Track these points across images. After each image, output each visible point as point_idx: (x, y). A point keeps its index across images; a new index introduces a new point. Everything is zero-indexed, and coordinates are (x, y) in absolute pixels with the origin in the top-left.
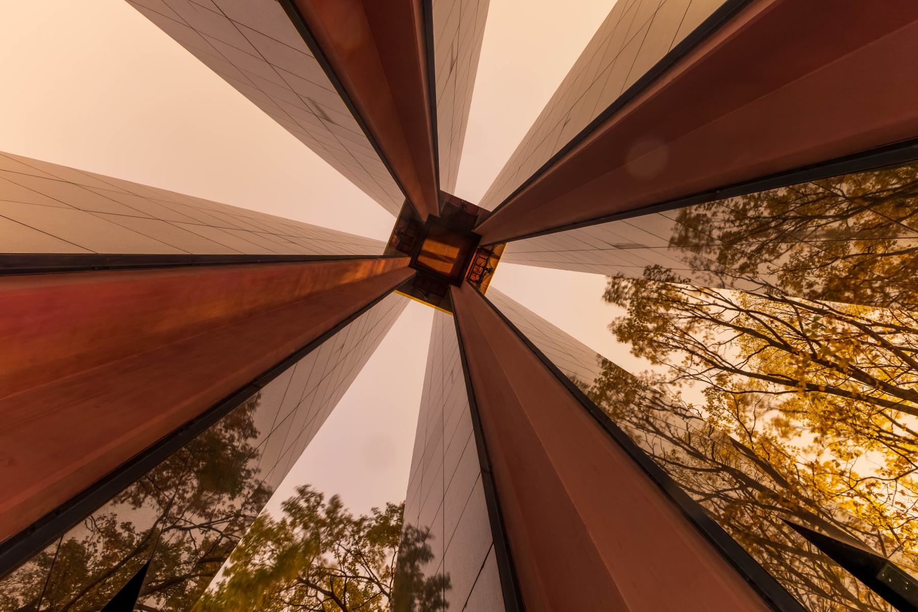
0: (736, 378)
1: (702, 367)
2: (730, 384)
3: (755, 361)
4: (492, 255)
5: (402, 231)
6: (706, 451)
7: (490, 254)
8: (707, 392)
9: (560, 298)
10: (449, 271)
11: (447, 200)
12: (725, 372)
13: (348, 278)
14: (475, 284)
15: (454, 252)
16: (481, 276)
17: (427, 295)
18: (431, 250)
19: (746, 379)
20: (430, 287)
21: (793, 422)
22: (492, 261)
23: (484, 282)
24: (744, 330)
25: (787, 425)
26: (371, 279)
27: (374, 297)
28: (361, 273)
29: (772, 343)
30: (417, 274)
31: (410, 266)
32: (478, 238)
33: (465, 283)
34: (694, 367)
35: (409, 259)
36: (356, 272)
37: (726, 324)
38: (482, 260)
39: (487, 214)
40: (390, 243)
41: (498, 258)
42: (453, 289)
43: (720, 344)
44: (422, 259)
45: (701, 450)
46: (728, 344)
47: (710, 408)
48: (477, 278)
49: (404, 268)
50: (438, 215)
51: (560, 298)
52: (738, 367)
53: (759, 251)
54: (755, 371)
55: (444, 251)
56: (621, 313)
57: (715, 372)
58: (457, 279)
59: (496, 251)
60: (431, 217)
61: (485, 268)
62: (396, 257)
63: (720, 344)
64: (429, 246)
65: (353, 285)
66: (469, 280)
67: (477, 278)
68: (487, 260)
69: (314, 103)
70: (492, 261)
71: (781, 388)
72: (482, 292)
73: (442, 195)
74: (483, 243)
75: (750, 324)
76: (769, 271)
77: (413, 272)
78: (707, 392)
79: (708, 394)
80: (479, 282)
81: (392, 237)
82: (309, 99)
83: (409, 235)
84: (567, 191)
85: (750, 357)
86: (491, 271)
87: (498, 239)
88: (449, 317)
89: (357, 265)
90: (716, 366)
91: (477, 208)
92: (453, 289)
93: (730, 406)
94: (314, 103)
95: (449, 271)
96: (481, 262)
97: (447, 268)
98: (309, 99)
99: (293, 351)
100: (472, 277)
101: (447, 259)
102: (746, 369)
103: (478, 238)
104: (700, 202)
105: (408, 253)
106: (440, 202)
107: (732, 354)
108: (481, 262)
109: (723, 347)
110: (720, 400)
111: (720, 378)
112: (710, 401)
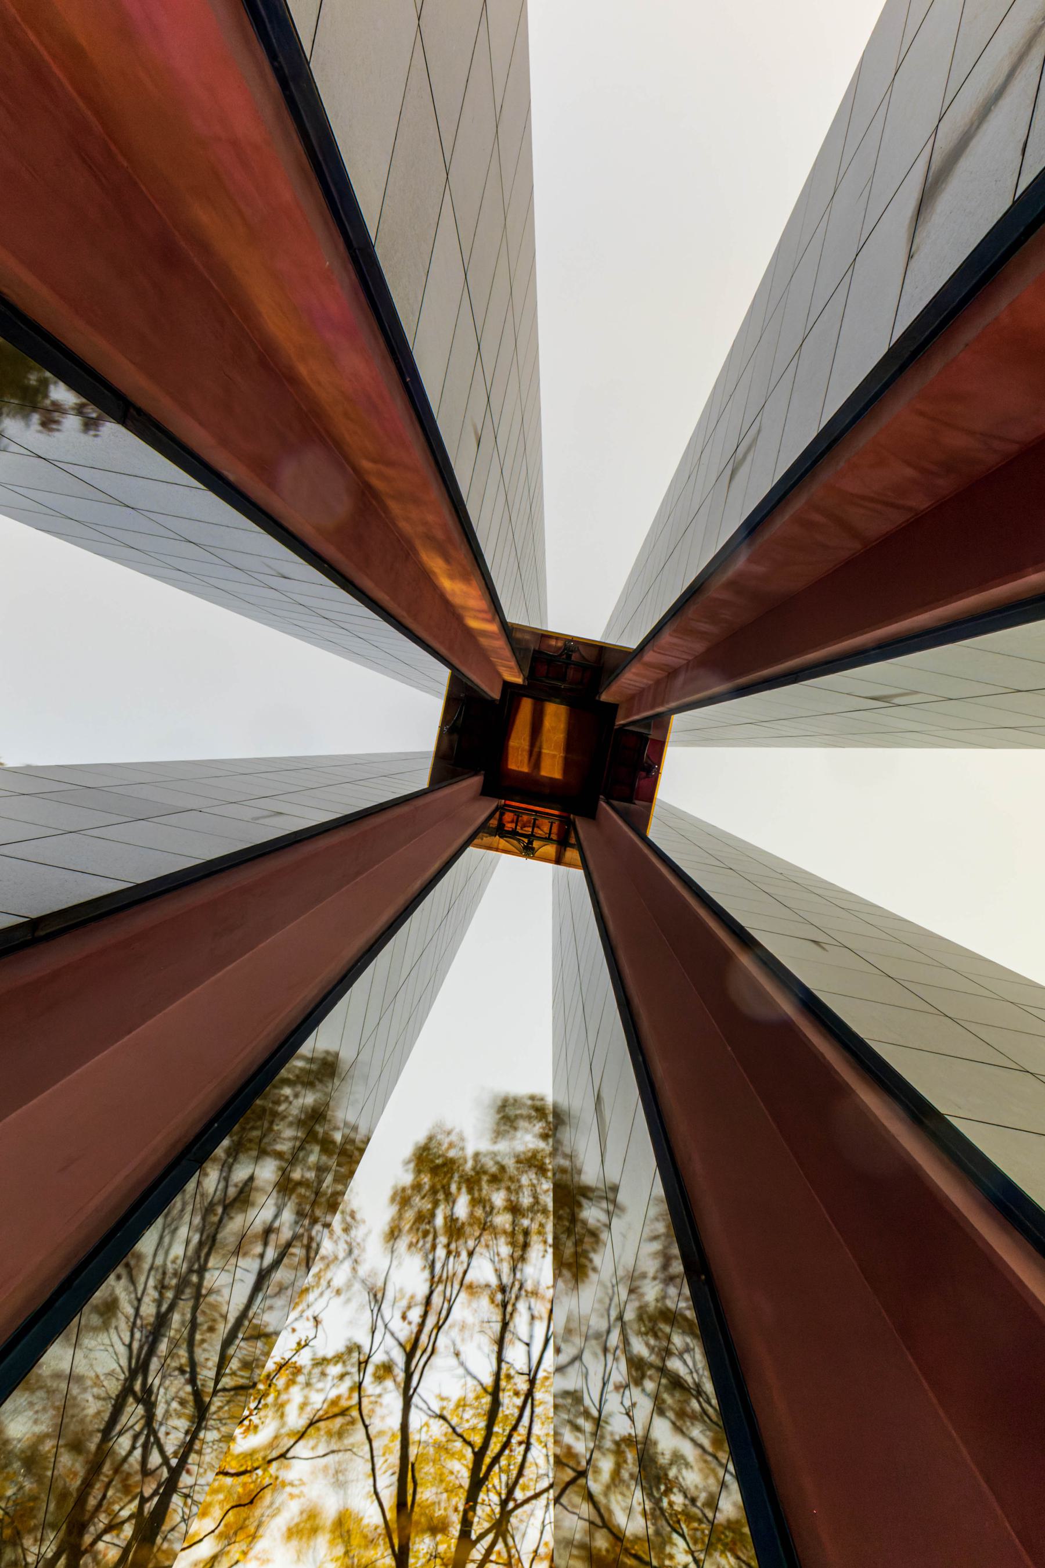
0: (393, 1400)
1: (404, 1331)
2: (378, 1390)
3: (438, 1430)
4: (564, 845)
5: (575, 657)
6: (233, 1374)
7: (563, 843)
8: (354, 1348)
9: (491, 1004)
10: (512, 766)
11: (653, 735)
12: (401, 1376)
13: (436, 564)
14: (494, 823)
15: (552, 768)
16: (513, 834)
17: (451, 731)
18: (548, 722)
19: (395, 1422)
20: (472, 734)
21: (322, 1541)
22: (550, 849)
23: (503, 843)
24: (495, 1392)
25: (314, 1531)
26: (452, 613)
27: (409, 622)
28: (453, 587)
29: (479, 1456)
30: (493, 701)
31: (507, 685)
32: (591, 813)
33: (492, 804)
34: (398, 1315)
35: (519, 680)
36: (451, 577)
37: (500, 1360)
38: (546, 829)
39: (639, 823)
40: (545, 636)
41: (558, 861)
42: (475, 782)
43: (457, 1355)
44: (526, 706)
45: (234, 1364)
46: (461, 1371)
47: (321, 1362)
48: (509, 826)
49: (499, 675)
50: (620, 722)
51: (491, 1004)
52: (415, 1400)
53: (676, 1383)
54: (414, 1437)
55: (553, 747)
56: (474, 1139)
57: (399, 1358)
58: (500, 785)
59: (572, 854)
60: (612, 709)
61: (531, 837)
62: (514, 650)
63: (457, 1355)
64: (556, 717)
65: (426, 577)
66: (501, 810)
67: (509, 826)
68: (548, 839)
69: (755, 440)
70: (550, 849)
71: (389, 1496)
72: (476, 841)
73: (661, 722)
74: (580, 824)
75: (510, 1404)
76: (629, 1412)
77: (496, 694)
78: (354, 1348)
79: (350, 1350)
80: (500, 831)
81: (557, 637)
82: (759, 431)
83: (570, 671)
84: (687, 977)
85: (442, 1417)
86: (528, 851)
87: (588, 854)
88: (423, 782)
89: (465, 578)
90: (410, 1356)
91: (650, 798)
92: (475, 782)
93: (334, 1403)
94: (755, 440)
95: (512, 766)
96: (545, 827)
97: (518, 762)
98: (759, 431)
99: (232, 477)
100: (508, 816)
101: (535, 756)
102: (416, 1419)
103: (591, 813)
104: (554, 1254)
105: (531, 676)
106: (646, 722)
107: (445, 1383)
108: (545, 827)
109: (454, 1361)
110: (342, 1377)
111: (387, 1368)
112: (338, 1358)
